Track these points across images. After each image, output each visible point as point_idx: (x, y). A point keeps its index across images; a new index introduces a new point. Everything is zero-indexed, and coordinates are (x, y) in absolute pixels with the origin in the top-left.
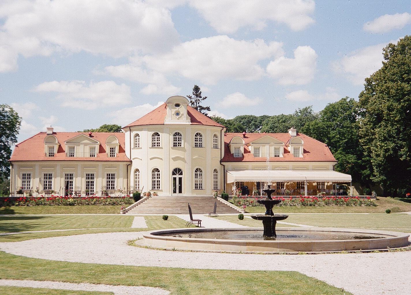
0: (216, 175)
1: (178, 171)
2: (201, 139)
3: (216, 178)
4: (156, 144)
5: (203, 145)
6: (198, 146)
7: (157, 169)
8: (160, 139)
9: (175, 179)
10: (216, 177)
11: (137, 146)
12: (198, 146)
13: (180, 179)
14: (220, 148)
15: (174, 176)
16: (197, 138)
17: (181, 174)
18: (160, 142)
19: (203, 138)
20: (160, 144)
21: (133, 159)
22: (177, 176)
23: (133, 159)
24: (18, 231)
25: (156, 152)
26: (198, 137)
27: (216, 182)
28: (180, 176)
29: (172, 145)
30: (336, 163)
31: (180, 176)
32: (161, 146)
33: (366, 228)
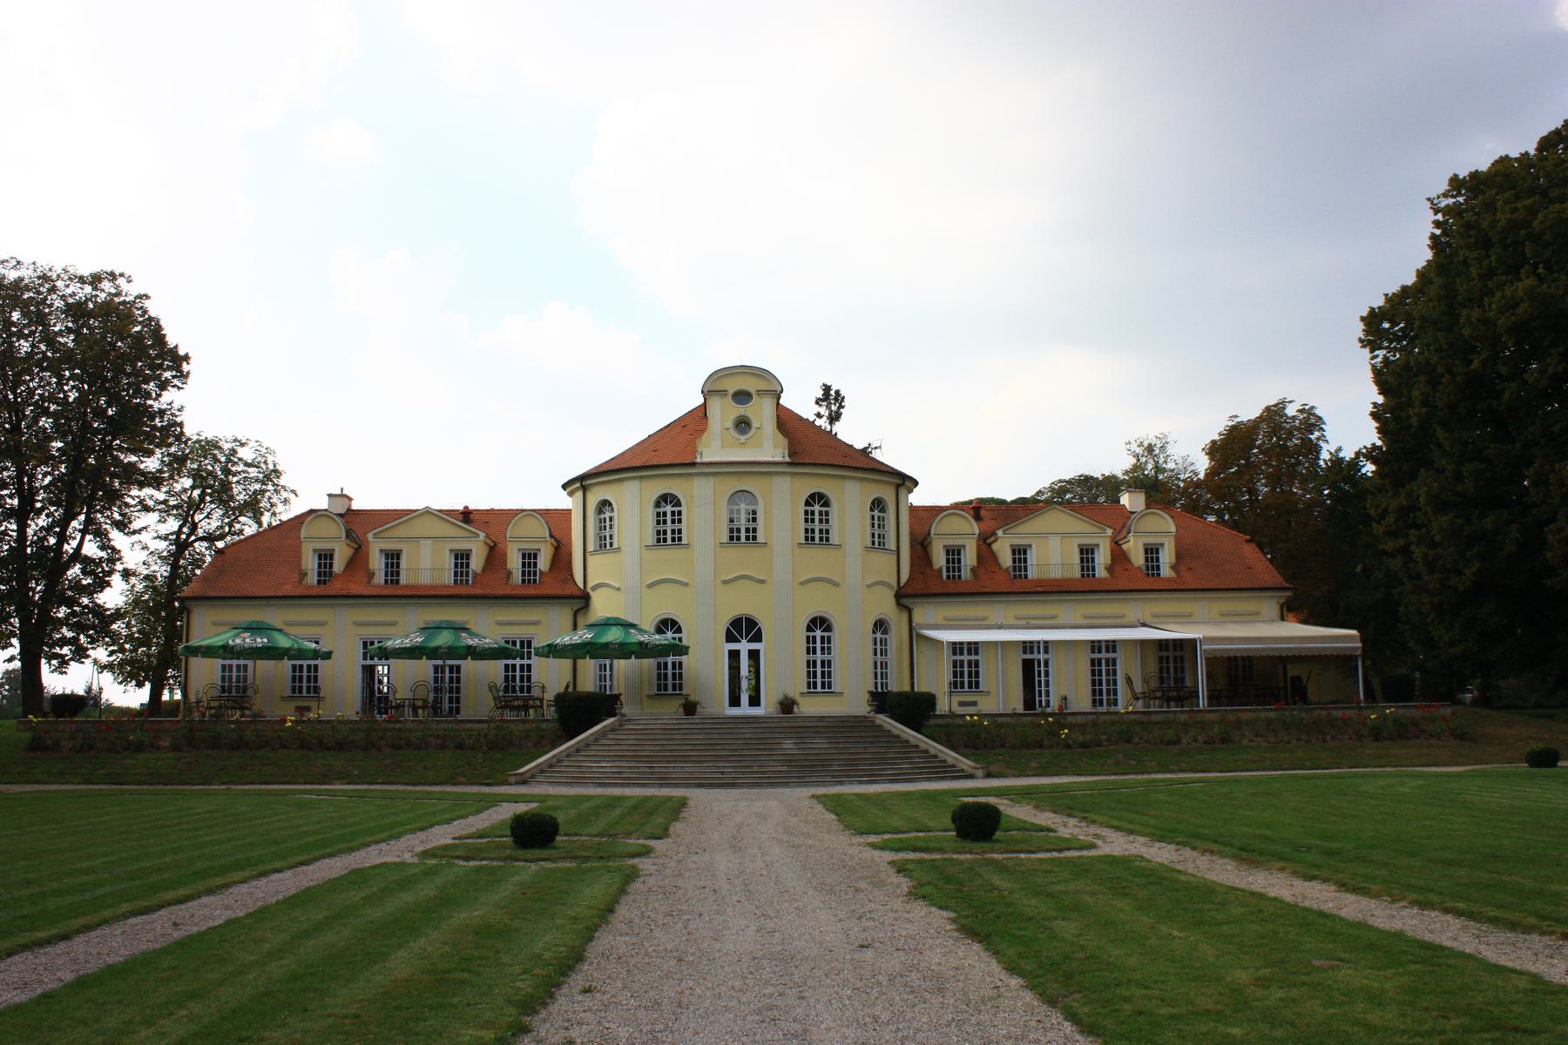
0: (884, 642)
1: (744, 628)
2: (827, 513)
3: (884, 653)
4: (816, 534)
5: (835, 538)
6: (743, 539)
7: (674, 623)
8: (684, 517)
9: (734, 655)
10: (880, 648)
11: (604, 544)
12: (743, 539)
13: (754, 655)
14: (893, 547)
15: (734, 646)
16: (813, 513)
17: (758, 638)
18: (684, 526)
19: (834, 511)
20: (684, 535)
21: (594, 588)
22: (744, 647)
23: (594, 588)
24: (548, 941)
25: (741, 559)
26: (817, 508)
27: (884, 665)
28: (754, 646)
29: (650, 538)
30: (1288, 594)
31: (754, 646)
32: (760, 539)
33: (1155, 781)
